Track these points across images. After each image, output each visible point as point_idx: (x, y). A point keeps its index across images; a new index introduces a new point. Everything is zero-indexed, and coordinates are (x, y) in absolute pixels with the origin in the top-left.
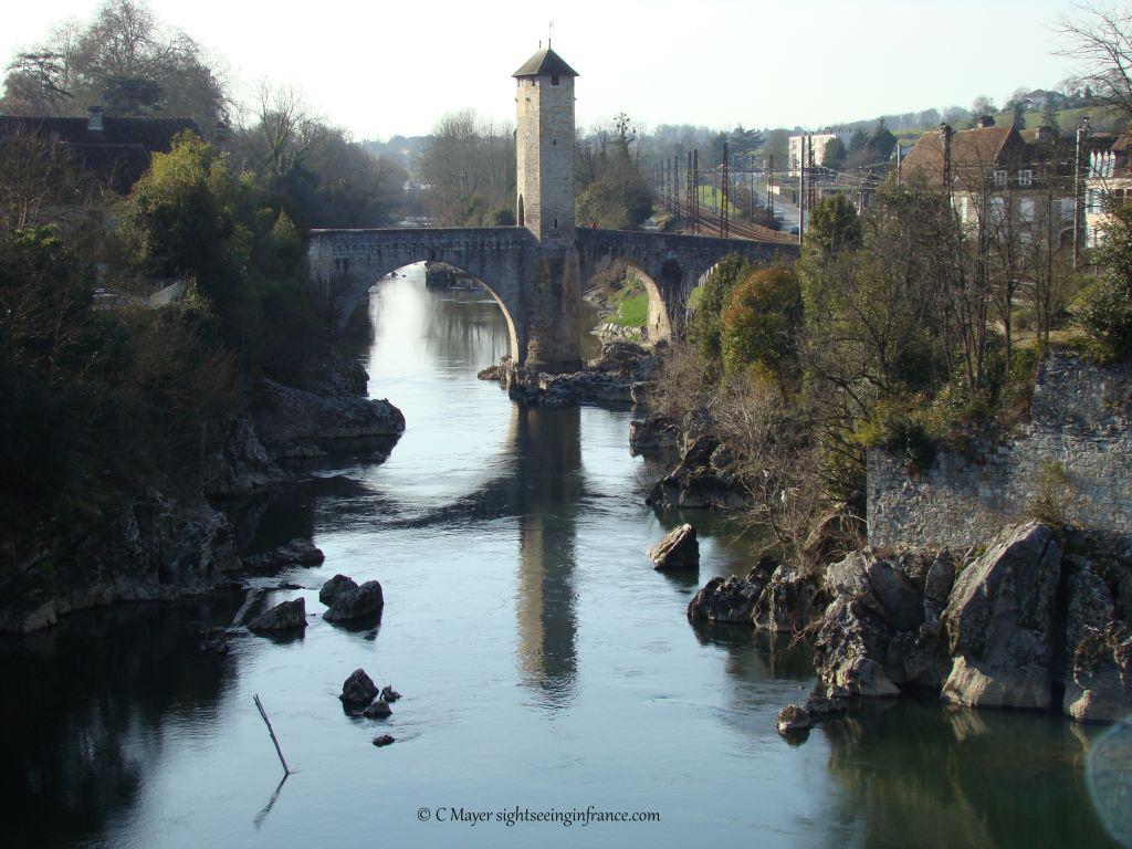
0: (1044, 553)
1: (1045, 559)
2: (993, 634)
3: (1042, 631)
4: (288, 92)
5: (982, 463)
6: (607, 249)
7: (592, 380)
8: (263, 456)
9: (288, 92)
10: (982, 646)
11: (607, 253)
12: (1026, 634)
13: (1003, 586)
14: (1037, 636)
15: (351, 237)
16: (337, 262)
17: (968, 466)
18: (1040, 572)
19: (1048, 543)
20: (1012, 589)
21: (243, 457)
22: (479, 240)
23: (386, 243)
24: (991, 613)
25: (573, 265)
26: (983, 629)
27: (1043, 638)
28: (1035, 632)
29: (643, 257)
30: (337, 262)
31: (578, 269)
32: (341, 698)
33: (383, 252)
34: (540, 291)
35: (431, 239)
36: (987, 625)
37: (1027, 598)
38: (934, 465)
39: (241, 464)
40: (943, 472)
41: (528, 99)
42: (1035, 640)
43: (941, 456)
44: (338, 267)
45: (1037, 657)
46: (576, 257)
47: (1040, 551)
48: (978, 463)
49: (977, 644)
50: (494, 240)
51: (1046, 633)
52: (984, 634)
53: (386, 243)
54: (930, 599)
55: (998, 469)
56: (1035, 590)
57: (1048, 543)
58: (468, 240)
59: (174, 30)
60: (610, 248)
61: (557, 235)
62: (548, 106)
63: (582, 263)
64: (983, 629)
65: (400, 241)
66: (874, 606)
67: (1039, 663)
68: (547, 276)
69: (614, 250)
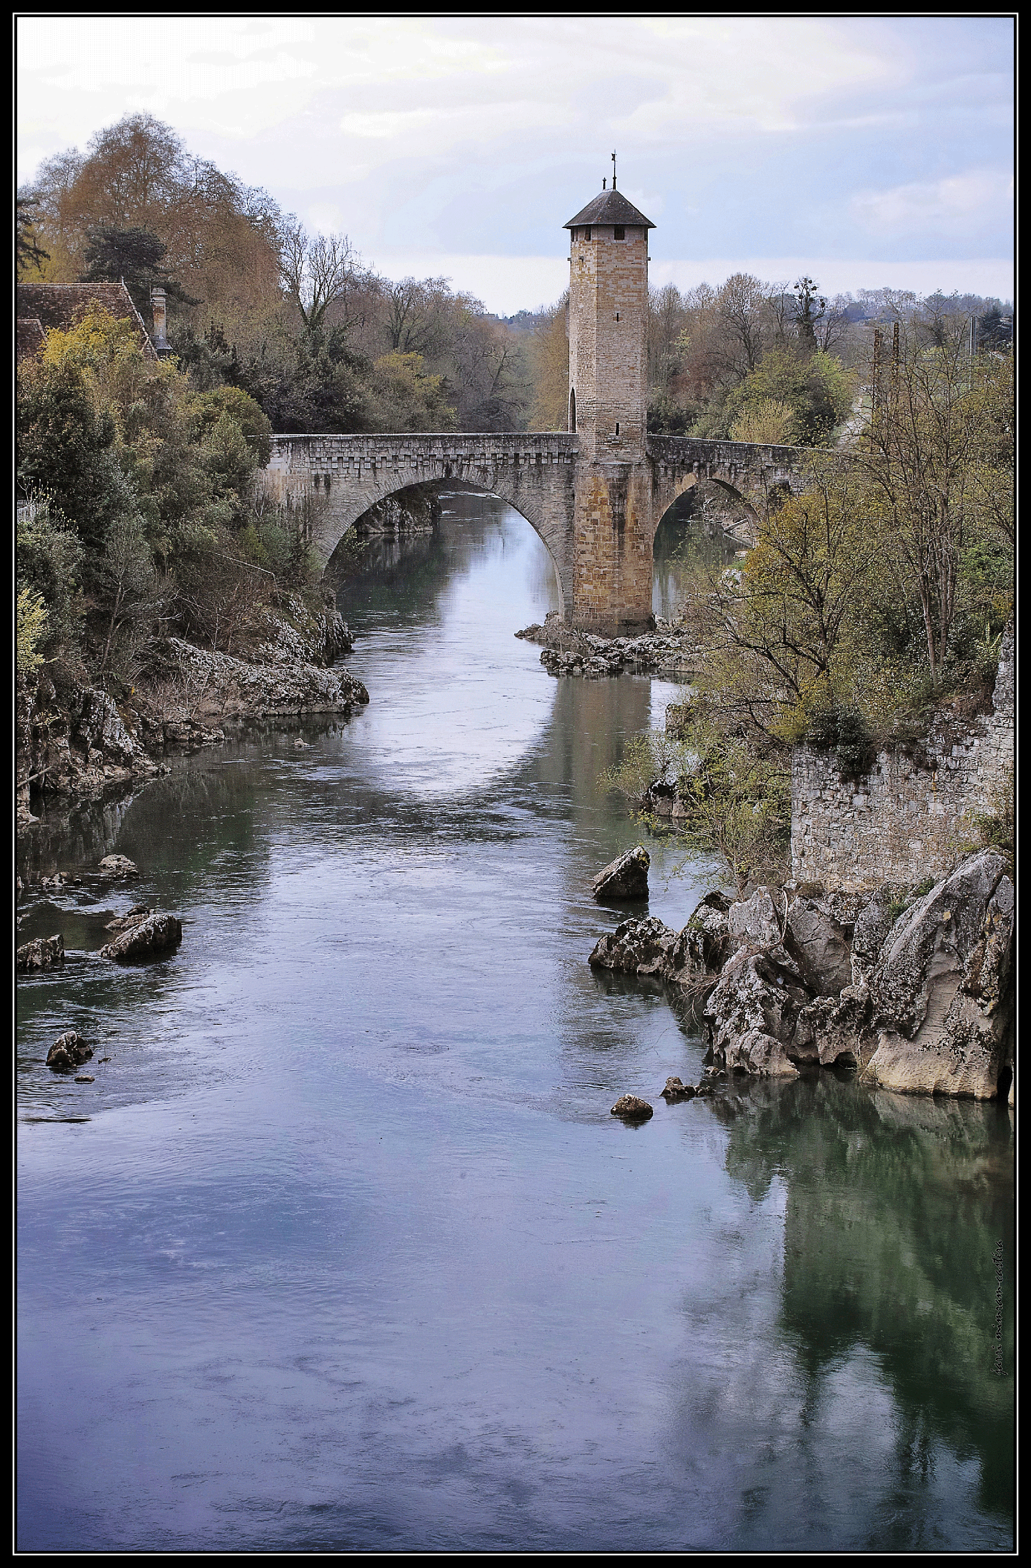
0: (993, 893)
1: (993, 900)
2: (928, 1003)
3: (988, 999)
4: (328, 248)
5: (935, 766)
6: (691, 465)
7: (656, 647)
8: (128, 744)
9: (328, 248)
10: (912, 1019)
11: (690, 471)
12: (970, 1004)
13: (940, 937)
14: (982, 1006)
15: (335, 445)
16: (317, 479)
17: (916, 773)
18: (988, 920)
19: (1000, 878)
20: (953, 941)
21: (98, 744)
22: (512, 452)
23: (384, 454)
24: (923, 974)
25: (641, 487)
26: (913, 996)
27: (988, 1009)
28: (980, 1000)
29: (742, 477)
30: (317, 479)
31: (650, 492)
32: (668, 1103)
33: (378, 465)
34: (595, 522)
35: (445, 449)
36: (919, 991)
37: (971, 954)
38: (874, 768)
39: (95, 753)
40: (886, 778)
41: (581, 258)
42: (980, 1012)
43: (883, 757)
44: (317, 487)
45: (980, 1036)
46: (646, 475)
47: (987, 890)
48: (928, 769)
49: (905, 1016)
50: (532, 451)
51: (992, 1002)
52: (914, 1003)
53: (384, 454)
54: (859, 954)
55: (952, 777)
56: (980, 944)
57: (1000, 878)
58: (496, 451)
59: (203, 168)
60: (696, 464)
61: (618, 445)
62: (608, 268)
63: (655, 485)
64: (913, 996)
65: (403, 452)
66: (785, 963)
67: (982, 1044)
68: (603, 502)
69: (702, 466)
